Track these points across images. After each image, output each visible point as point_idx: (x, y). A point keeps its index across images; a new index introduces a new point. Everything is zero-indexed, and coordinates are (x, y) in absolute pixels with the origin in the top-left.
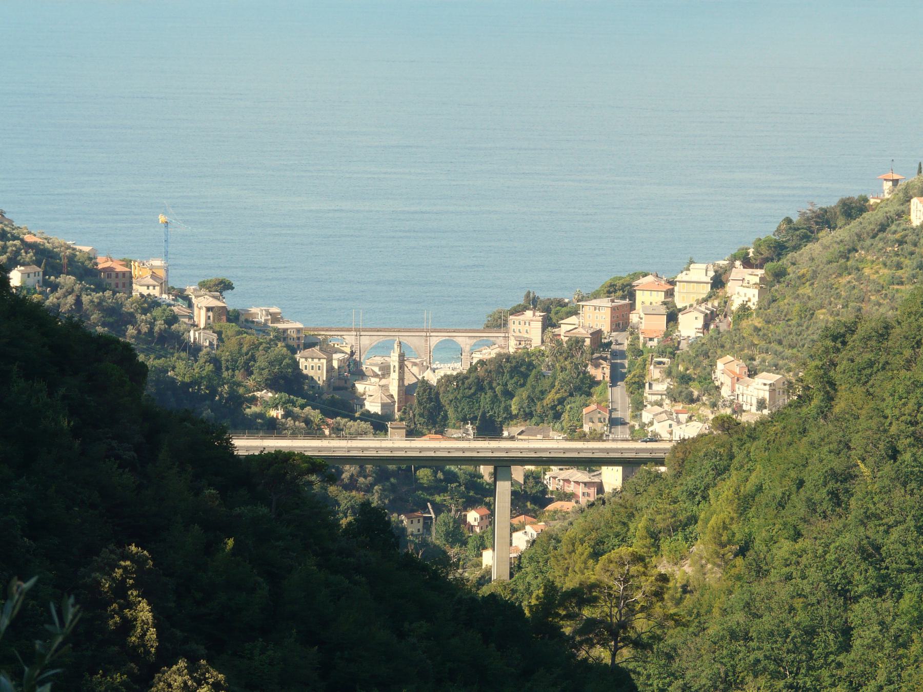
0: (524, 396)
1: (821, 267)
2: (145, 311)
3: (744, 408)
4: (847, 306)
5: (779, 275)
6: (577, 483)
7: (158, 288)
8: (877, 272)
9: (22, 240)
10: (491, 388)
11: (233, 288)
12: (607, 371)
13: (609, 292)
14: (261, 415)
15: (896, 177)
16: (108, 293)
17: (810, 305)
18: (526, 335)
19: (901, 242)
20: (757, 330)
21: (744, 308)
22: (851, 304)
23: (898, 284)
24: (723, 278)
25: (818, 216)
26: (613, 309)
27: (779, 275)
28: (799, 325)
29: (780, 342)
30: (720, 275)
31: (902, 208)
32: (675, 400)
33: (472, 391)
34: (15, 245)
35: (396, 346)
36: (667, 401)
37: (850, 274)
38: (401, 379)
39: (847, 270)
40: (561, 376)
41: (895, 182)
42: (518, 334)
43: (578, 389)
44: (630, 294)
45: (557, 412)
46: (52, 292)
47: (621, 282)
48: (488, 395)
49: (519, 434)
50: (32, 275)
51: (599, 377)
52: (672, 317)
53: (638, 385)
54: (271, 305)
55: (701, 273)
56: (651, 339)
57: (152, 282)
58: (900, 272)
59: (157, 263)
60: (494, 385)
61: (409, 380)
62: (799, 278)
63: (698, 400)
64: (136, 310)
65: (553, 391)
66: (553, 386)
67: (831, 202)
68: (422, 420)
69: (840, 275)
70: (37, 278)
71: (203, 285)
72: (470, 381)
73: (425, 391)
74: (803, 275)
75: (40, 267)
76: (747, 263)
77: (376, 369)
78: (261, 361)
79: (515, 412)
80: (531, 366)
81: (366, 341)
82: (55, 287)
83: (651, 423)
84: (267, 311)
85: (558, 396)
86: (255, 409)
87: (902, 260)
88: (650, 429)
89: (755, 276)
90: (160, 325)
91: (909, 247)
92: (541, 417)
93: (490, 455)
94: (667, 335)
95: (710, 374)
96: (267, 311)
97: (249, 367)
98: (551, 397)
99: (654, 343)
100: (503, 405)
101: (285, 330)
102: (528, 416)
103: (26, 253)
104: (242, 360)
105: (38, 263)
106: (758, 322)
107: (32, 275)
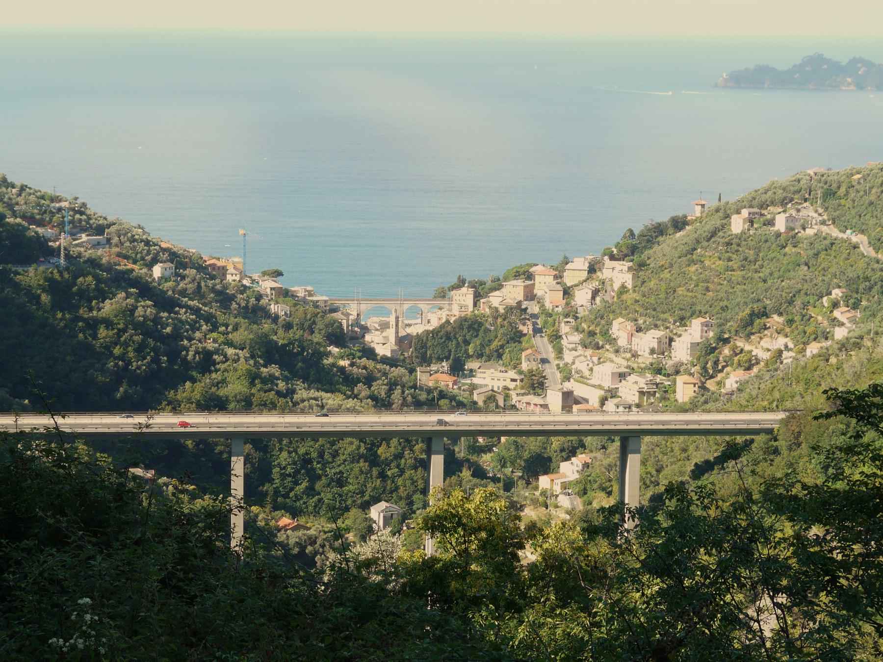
0: (478, 343)
1: (675, 260)
2: (242, 293)
3: (639, 353)
4: (698, 285)
5: (642, 265)
6: (536, 405)
7: (238, 276)
8: (715, 263)
9: (160, 246)
10: (455, 338)
11: (283, 275)
12: (531, 327)
13: (515, 276)
14: (334, 365)
15: (703, 203)
16: (218, 281)
17: (672, 284)
18: (463, 303)
19: (729, 244)
20: (637, 301)
21: (623, 287)
22: (701, 284)
23: (731, 271)
24: (596, 267)
25: (655, 228)
26: (525, 287)
27: (642, 265)
28: (666, 298)
29: (655, 310)
30: (593, 265)
31: (724, 222)
32: (586, 347)
33: (443, 340)
34: (156, 249)
35: (393, 312)
36: (580, 347)
37: (695, 264)
38: (397, 332)
39: (693, 262)
40: (501, 331)
41: (703, 206)
42: (458, 302)
43: (512, 339)
44: (530, 276)
45: (499, 353)
46: (181, 280)
47: (523, 269)
48: (454, 343)
49: (479, 368)
50: (168, 269)
51: (525, 332)
52: (567, 292)
53: (556, 338)
54: (307, 285)
55: (579, 266)
56: (557, 307)
57: (234, 272)
58: (730, 264)
59: (236, 260)
60: (457, 336)
61: (402, 333)
62: (660, 267)
63: (602, 347)
64: (237, 292)
65: (497, 340)
66: (496, 337)
67: (664, 218)
68: (418, 360)
69: (689, 265)
70: (171, 271)
71: (264, 273)
72: (442, 333)
73: (419, 341)
74: (663, 266)
75: (172, 263)
76: (612, 258)
77: (377, 326)
78: (320, 325)
79: (471, 353)
80: (480, 324)
81: (363, 307)
82: (183, 278)
83: (573, 363)
84: (305, 289)
85: (500, 343)
86: (331, 360)
87: (731, 255)
88: (573, 367)
89: (625, 265)
90: (253, 301)
91: (734, 247)
92: (488, 356)
93: (625, 427)
94: (567, 304)
95: (608, 330)
96: (305, 289)
97: (312, 329)
98: (495, 344)
99: (560, 309)
100: (463, 349)
101: (317, 301)
102: (480, 356)
103: (164, 254)
104: (307, 324)
105: (172, 261)
106: (636, 296)
107: (168, 269)
